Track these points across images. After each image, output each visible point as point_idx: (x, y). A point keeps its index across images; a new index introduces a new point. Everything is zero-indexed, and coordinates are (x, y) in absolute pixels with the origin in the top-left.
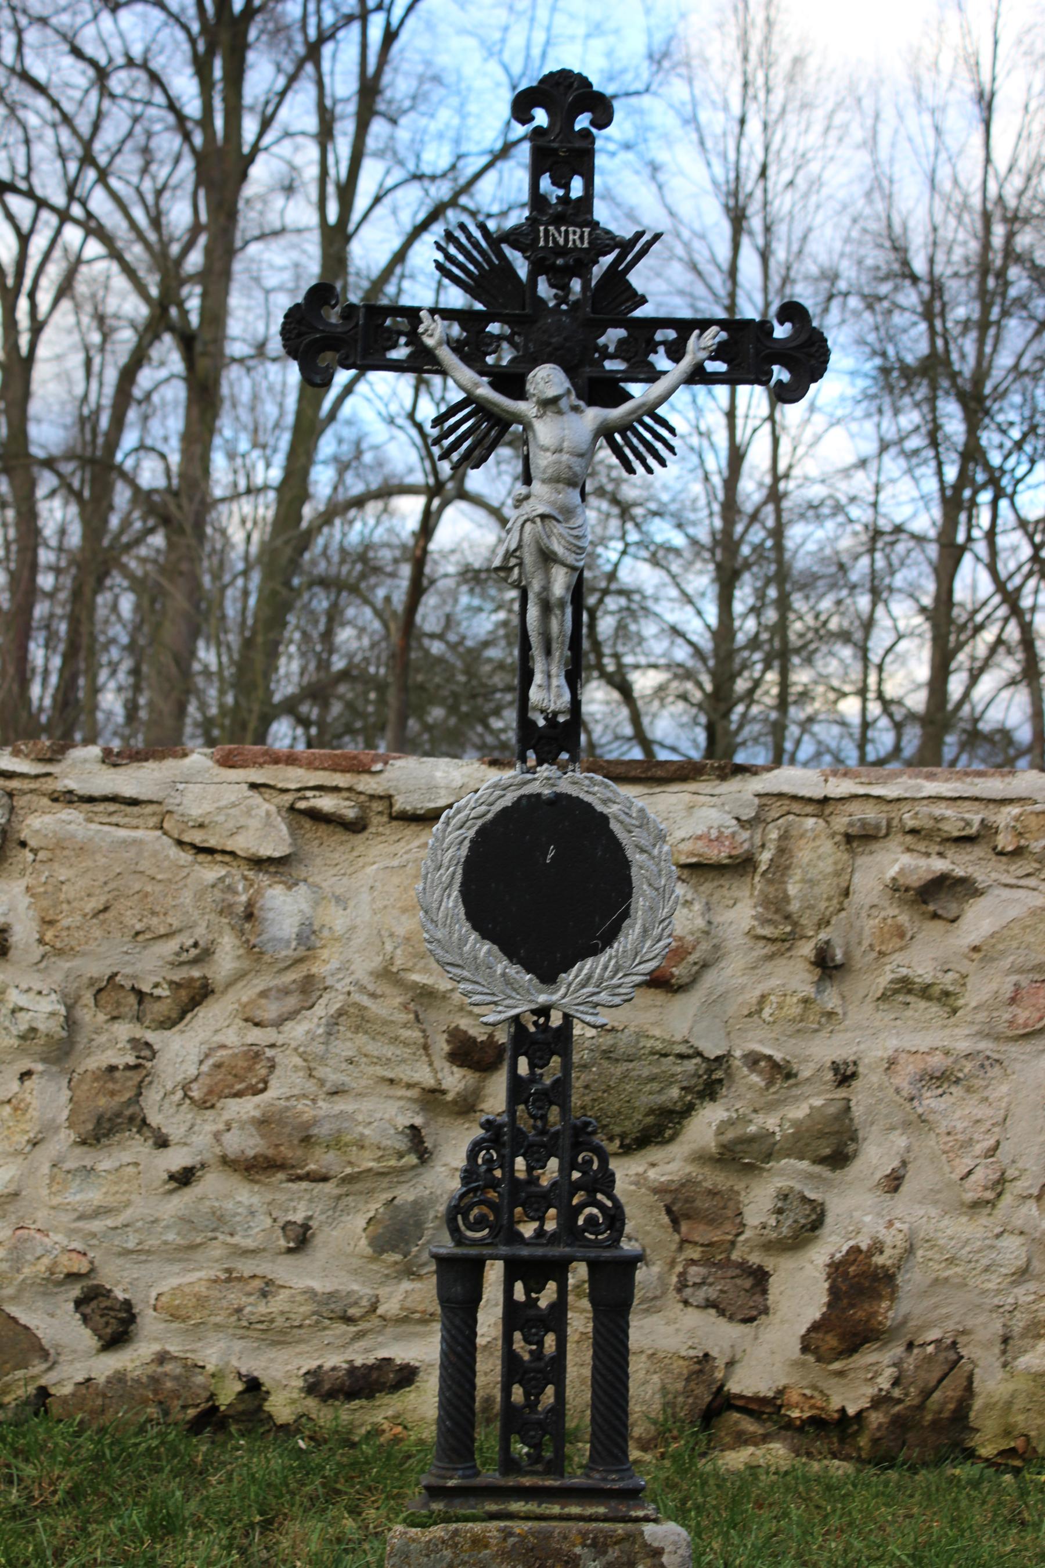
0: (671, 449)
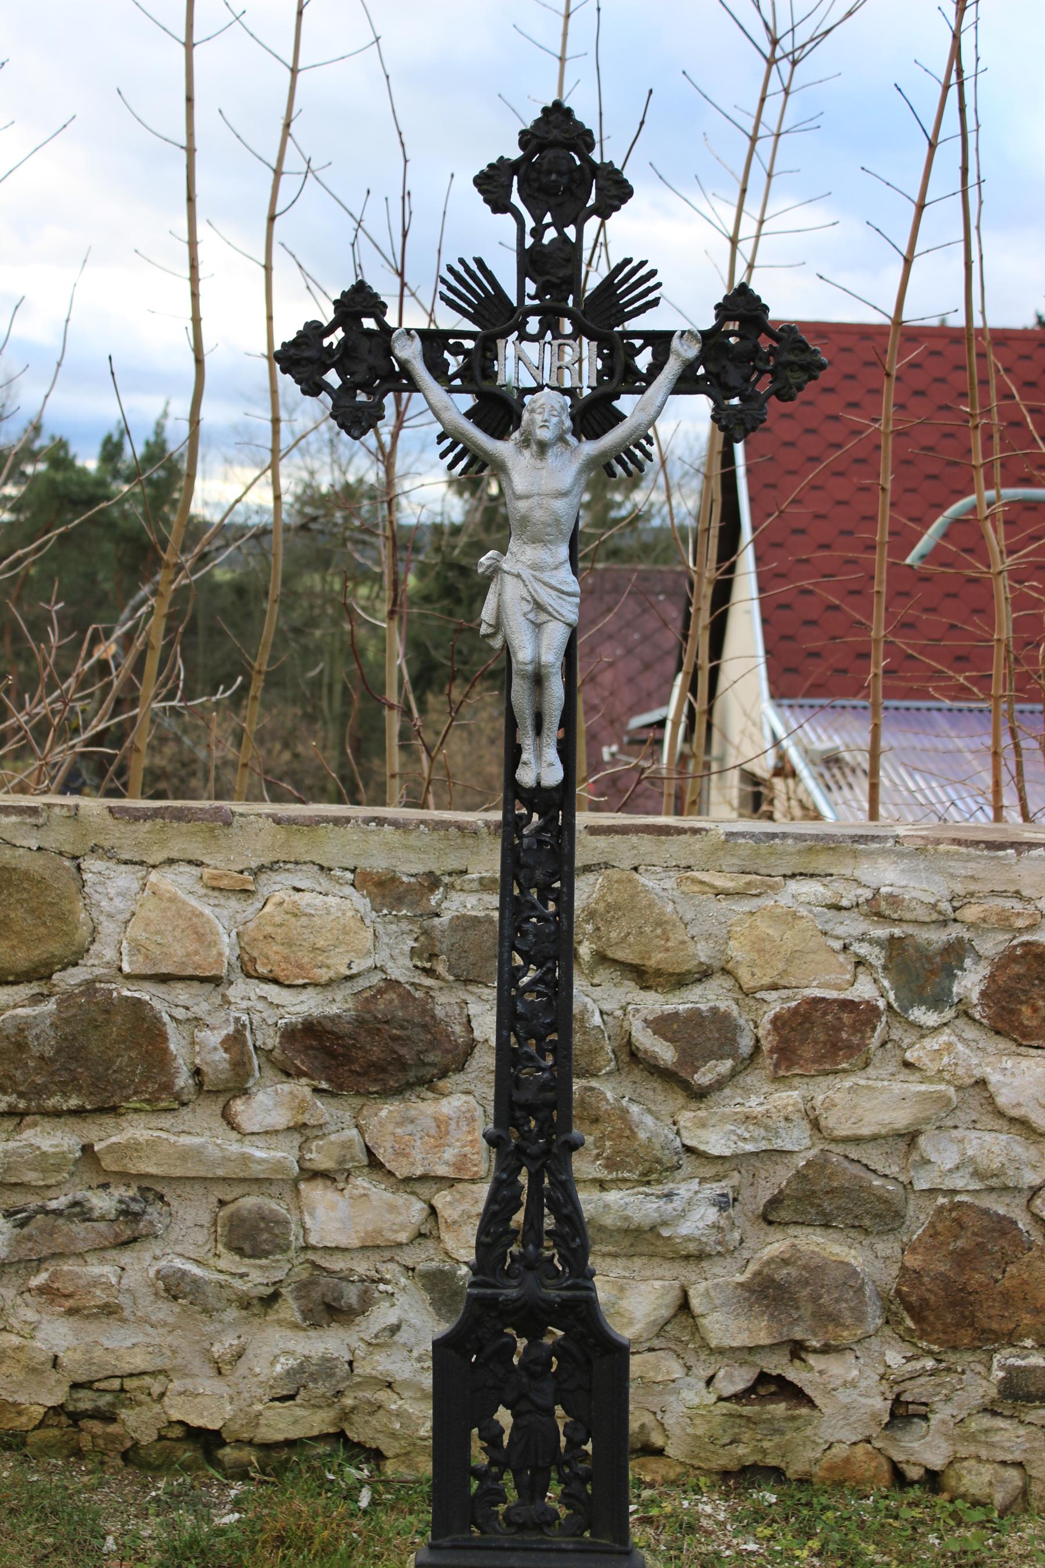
0: (643, 264)
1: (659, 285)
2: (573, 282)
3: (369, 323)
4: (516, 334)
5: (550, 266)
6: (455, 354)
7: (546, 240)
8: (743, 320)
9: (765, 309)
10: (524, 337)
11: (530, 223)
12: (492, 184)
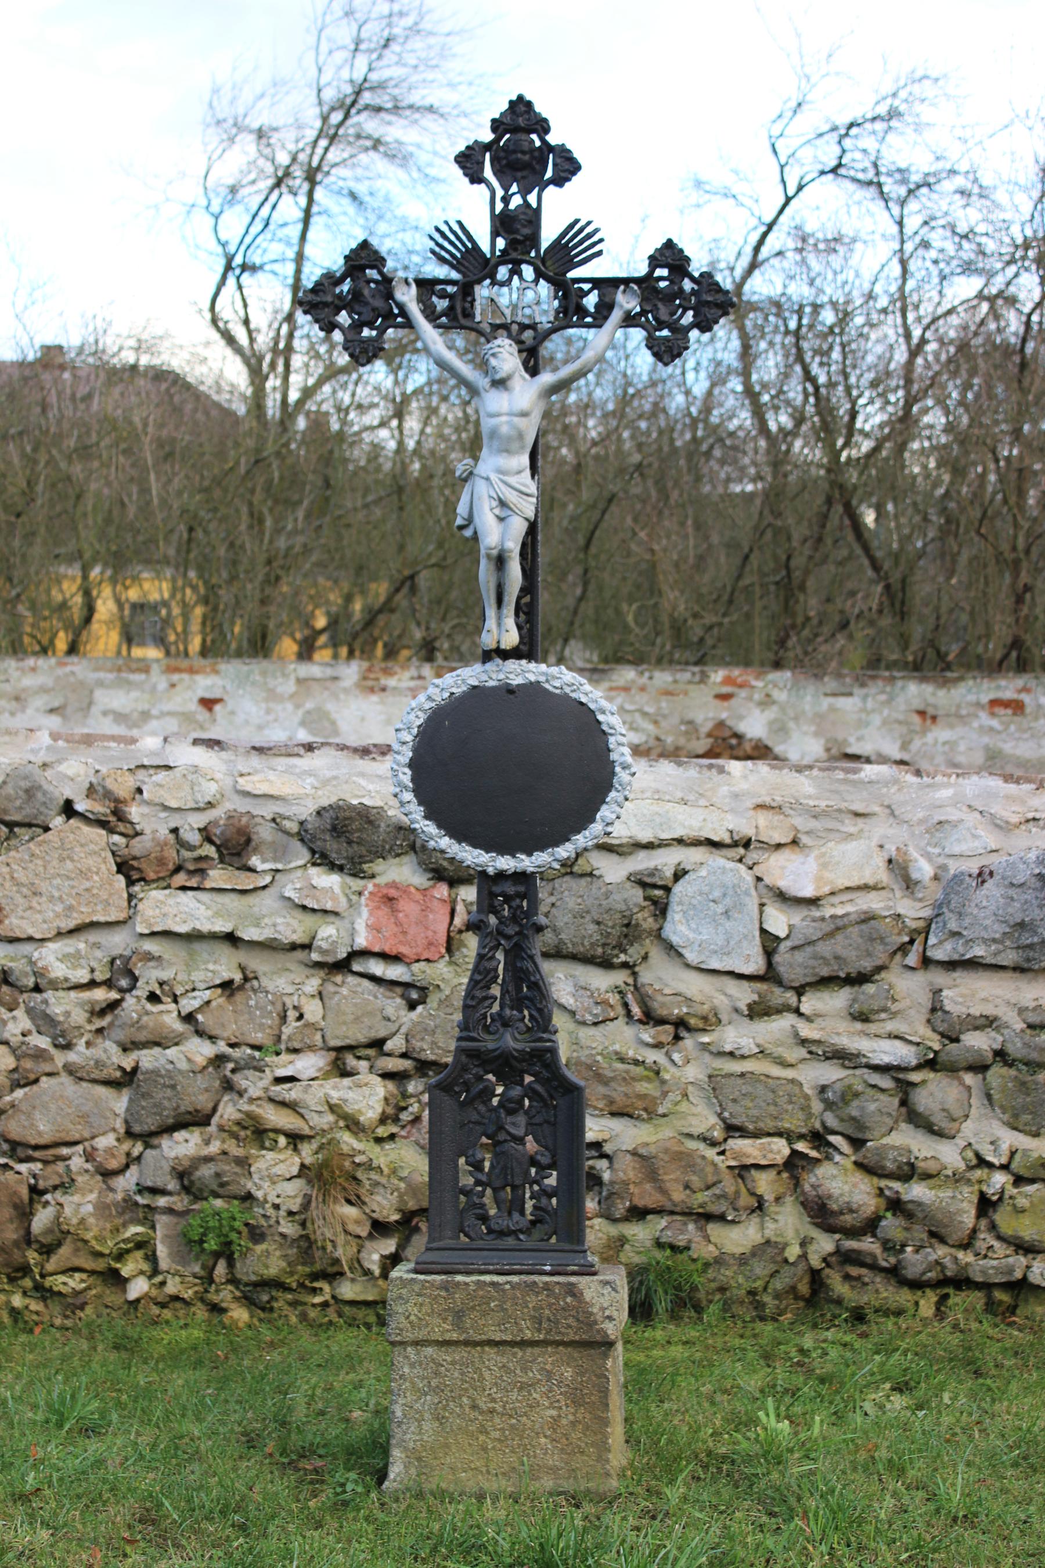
0: (589, 223)
1: (601, 240)
2: (534, 239)
3: (372, 273)
4: (488, 281)
5: (517, 228)
6: (441, 297)
7: (512, 206)
8: (672, 268)
9: (688, 260)
10: (494, 283)
11: (500, 193)
12: (469, 161)
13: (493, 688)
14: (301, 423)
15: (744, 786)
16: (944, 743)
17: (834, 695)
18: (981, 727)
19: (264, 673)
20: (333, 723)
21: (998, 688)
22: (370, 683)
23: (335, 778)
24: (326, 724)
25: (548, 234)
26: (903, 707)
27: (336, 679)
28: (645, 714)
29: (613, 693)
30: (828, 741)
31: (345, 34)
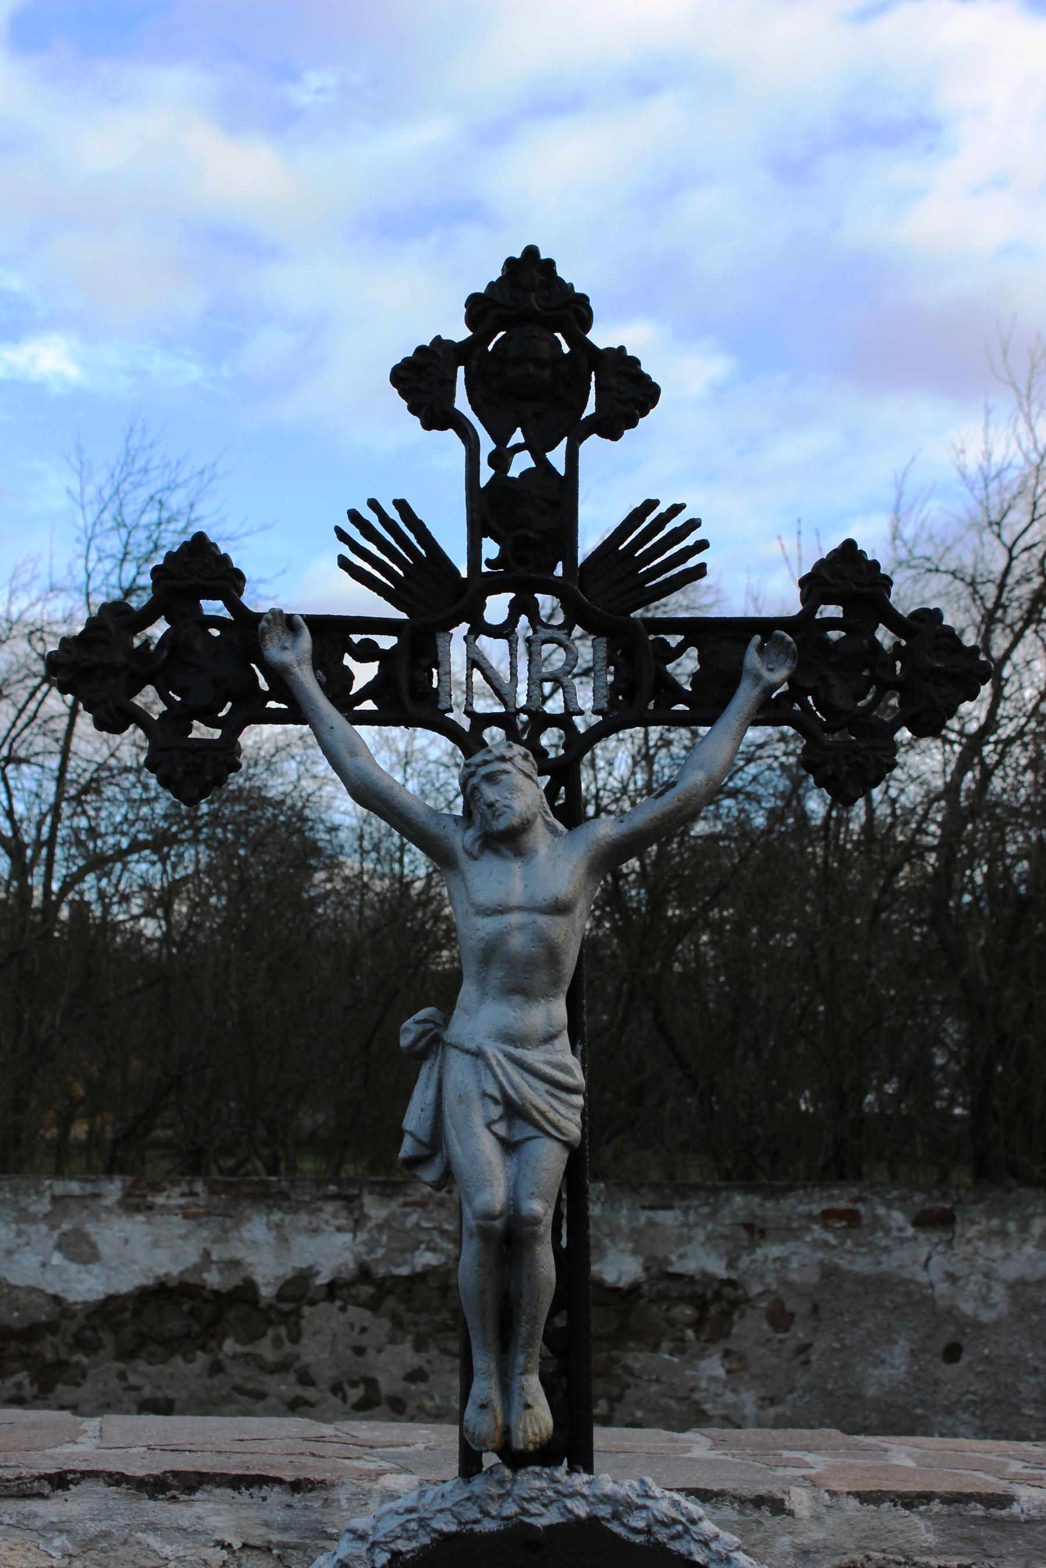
3: (213, 607)
5: (526, 516)
7: (514, 472)
10: (479, 628)
11: (487, 445)
12: (422, 381)
13: (491, 1536)
14: (64, 913)
15: (817, 1535)
16: (775, 1260)
17: (653, 1208)
18: (814, 1241)
19: (15, 1191)
20: (93, 1246)
21: (832, 1197)
22: (135, 1201)
23: (105, 1535)
24: (85, 1248)
25: (595, 524)
26: (728, 1221)
27: (97, 1196)
28: (443, 1233)
29: (408, 1209)
30: (646, 1260)
31: (114, 544)
